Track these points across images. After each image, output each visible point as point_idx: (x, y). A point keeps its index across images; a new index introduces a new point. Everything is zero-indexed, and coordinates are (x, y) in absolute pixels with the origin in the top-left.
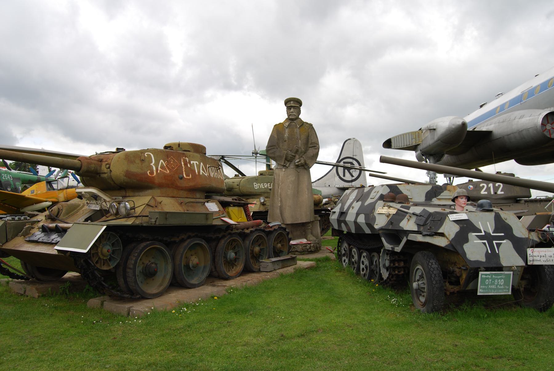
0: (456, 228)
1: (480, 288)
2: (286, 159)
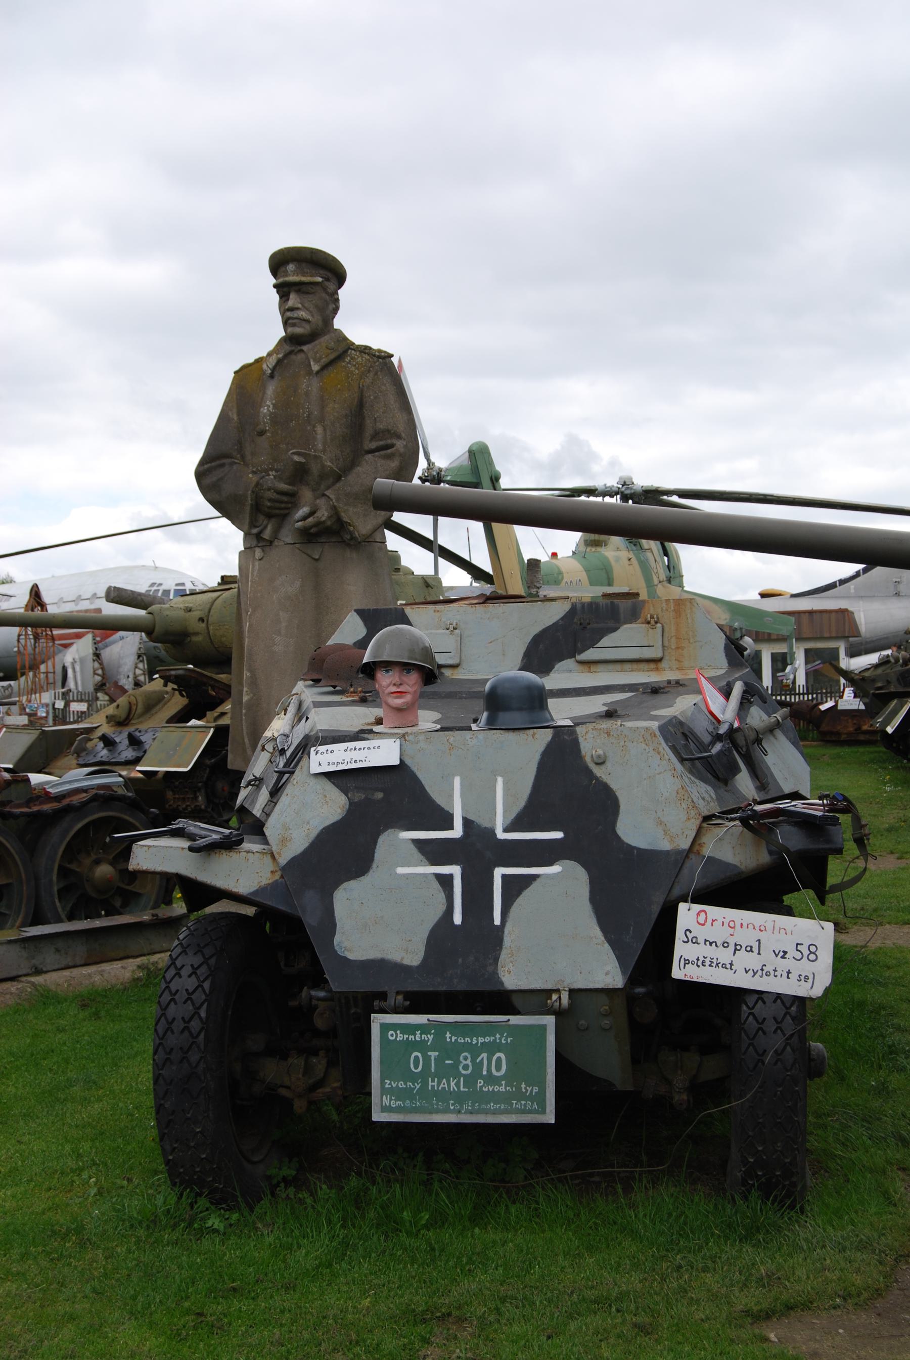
0: (331, 806)
1: (384, 1092)
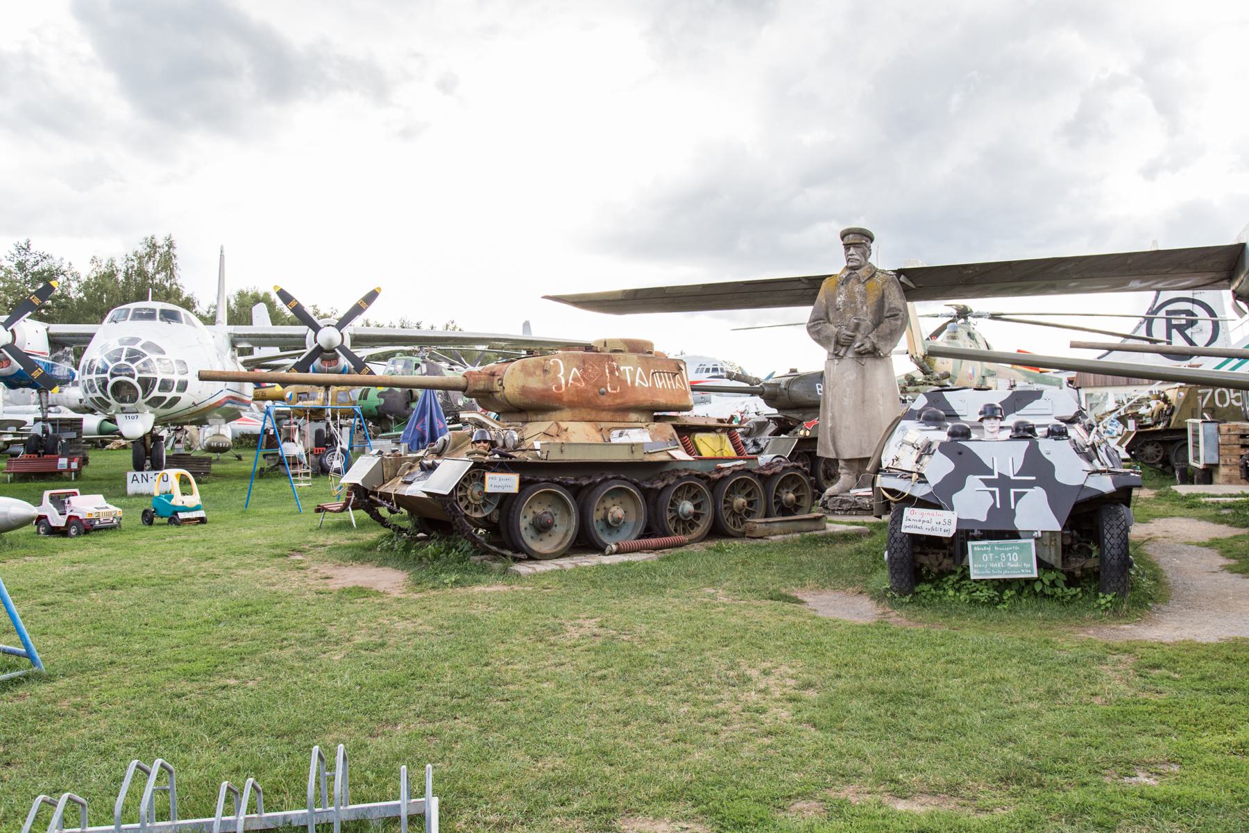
2: (837, 342)
